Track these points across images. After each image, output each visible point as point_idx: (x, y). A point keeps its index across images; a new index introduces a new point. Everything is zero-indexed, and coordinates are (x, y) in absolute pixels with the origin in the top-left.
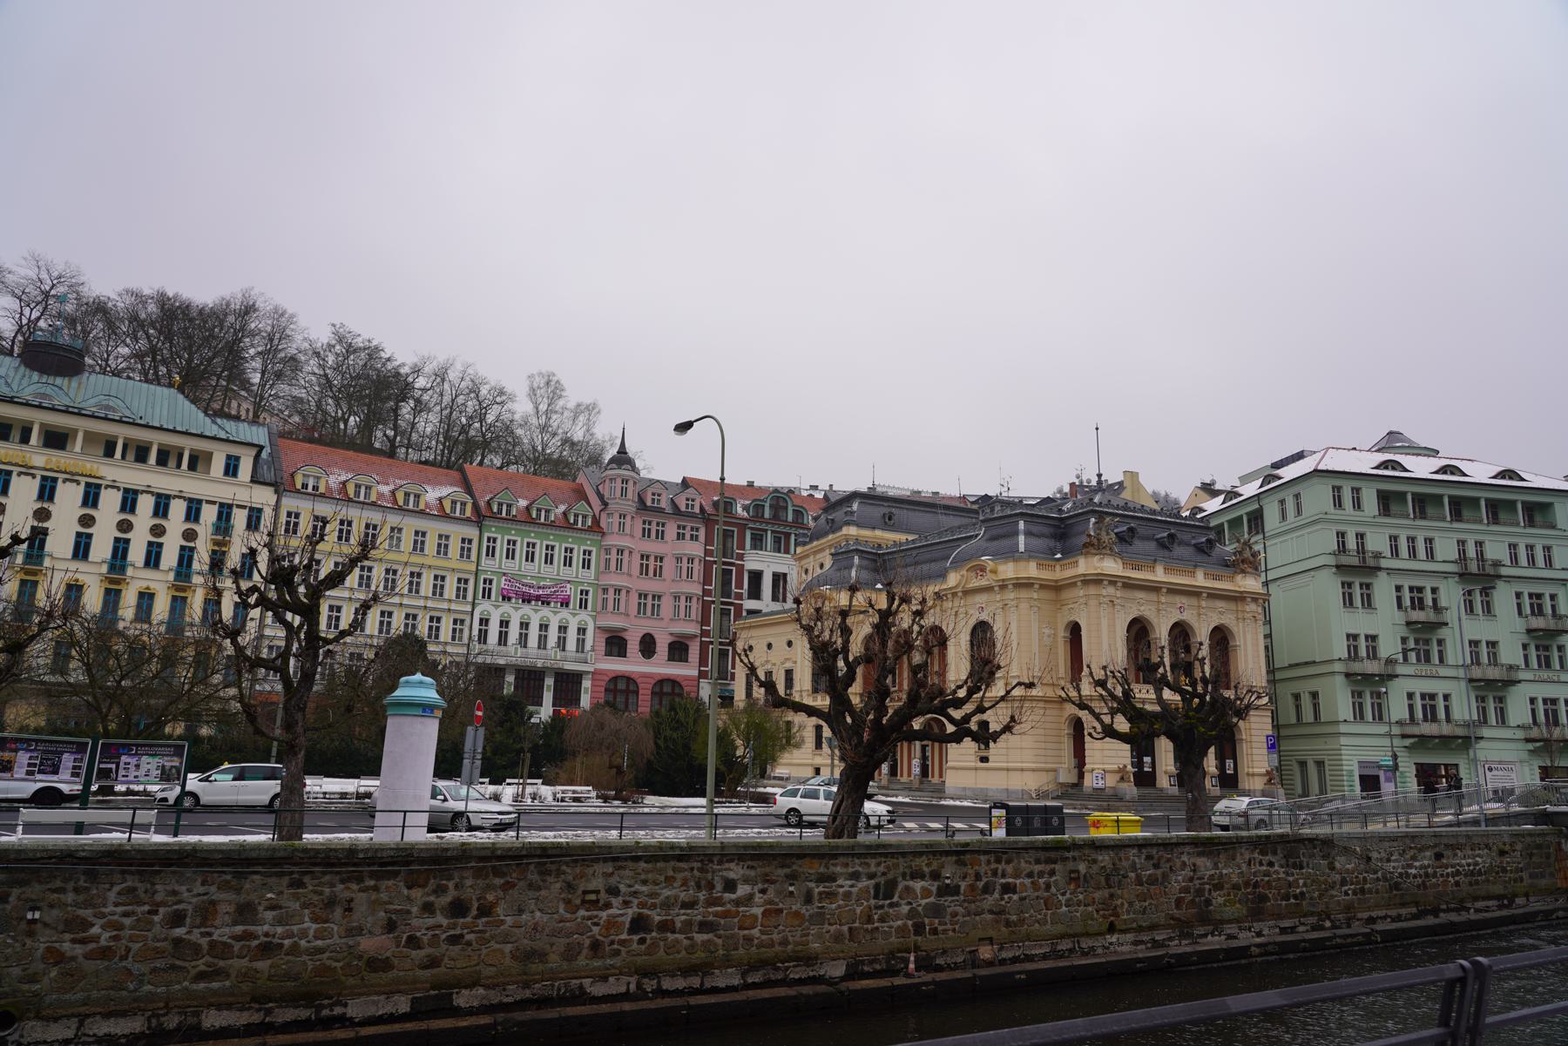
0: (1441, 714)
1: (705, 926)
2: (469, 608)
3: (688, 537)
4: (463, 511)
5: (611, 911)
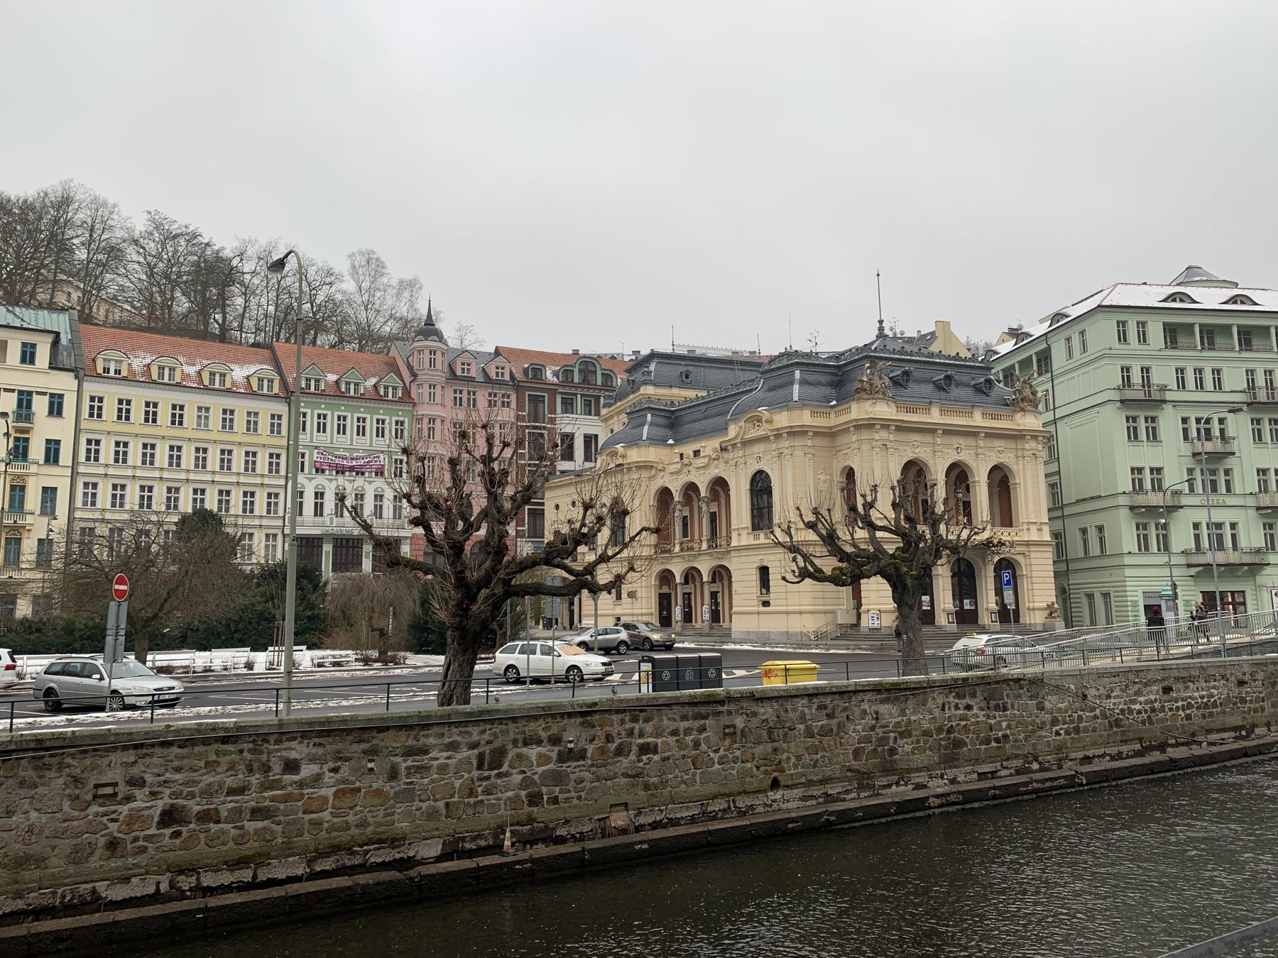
0: (1228, 542)
1: (257, 813)
2: (282, 482)
3: (499, 404)
4: (270, 388)
5: (133, 805)
